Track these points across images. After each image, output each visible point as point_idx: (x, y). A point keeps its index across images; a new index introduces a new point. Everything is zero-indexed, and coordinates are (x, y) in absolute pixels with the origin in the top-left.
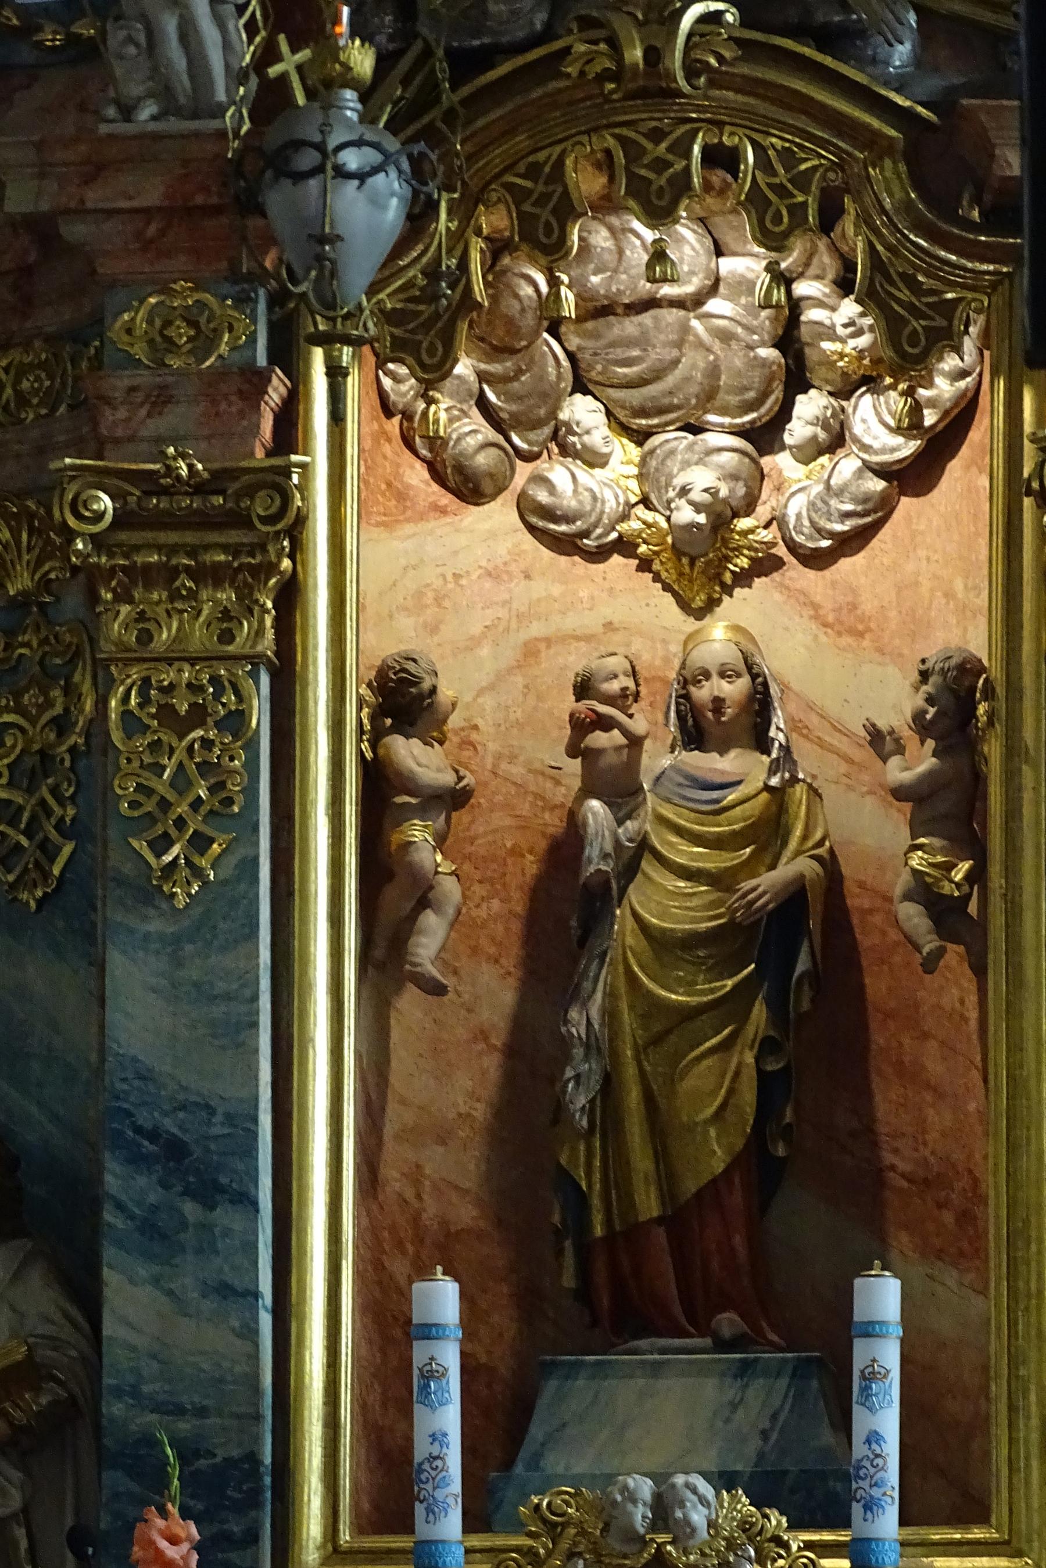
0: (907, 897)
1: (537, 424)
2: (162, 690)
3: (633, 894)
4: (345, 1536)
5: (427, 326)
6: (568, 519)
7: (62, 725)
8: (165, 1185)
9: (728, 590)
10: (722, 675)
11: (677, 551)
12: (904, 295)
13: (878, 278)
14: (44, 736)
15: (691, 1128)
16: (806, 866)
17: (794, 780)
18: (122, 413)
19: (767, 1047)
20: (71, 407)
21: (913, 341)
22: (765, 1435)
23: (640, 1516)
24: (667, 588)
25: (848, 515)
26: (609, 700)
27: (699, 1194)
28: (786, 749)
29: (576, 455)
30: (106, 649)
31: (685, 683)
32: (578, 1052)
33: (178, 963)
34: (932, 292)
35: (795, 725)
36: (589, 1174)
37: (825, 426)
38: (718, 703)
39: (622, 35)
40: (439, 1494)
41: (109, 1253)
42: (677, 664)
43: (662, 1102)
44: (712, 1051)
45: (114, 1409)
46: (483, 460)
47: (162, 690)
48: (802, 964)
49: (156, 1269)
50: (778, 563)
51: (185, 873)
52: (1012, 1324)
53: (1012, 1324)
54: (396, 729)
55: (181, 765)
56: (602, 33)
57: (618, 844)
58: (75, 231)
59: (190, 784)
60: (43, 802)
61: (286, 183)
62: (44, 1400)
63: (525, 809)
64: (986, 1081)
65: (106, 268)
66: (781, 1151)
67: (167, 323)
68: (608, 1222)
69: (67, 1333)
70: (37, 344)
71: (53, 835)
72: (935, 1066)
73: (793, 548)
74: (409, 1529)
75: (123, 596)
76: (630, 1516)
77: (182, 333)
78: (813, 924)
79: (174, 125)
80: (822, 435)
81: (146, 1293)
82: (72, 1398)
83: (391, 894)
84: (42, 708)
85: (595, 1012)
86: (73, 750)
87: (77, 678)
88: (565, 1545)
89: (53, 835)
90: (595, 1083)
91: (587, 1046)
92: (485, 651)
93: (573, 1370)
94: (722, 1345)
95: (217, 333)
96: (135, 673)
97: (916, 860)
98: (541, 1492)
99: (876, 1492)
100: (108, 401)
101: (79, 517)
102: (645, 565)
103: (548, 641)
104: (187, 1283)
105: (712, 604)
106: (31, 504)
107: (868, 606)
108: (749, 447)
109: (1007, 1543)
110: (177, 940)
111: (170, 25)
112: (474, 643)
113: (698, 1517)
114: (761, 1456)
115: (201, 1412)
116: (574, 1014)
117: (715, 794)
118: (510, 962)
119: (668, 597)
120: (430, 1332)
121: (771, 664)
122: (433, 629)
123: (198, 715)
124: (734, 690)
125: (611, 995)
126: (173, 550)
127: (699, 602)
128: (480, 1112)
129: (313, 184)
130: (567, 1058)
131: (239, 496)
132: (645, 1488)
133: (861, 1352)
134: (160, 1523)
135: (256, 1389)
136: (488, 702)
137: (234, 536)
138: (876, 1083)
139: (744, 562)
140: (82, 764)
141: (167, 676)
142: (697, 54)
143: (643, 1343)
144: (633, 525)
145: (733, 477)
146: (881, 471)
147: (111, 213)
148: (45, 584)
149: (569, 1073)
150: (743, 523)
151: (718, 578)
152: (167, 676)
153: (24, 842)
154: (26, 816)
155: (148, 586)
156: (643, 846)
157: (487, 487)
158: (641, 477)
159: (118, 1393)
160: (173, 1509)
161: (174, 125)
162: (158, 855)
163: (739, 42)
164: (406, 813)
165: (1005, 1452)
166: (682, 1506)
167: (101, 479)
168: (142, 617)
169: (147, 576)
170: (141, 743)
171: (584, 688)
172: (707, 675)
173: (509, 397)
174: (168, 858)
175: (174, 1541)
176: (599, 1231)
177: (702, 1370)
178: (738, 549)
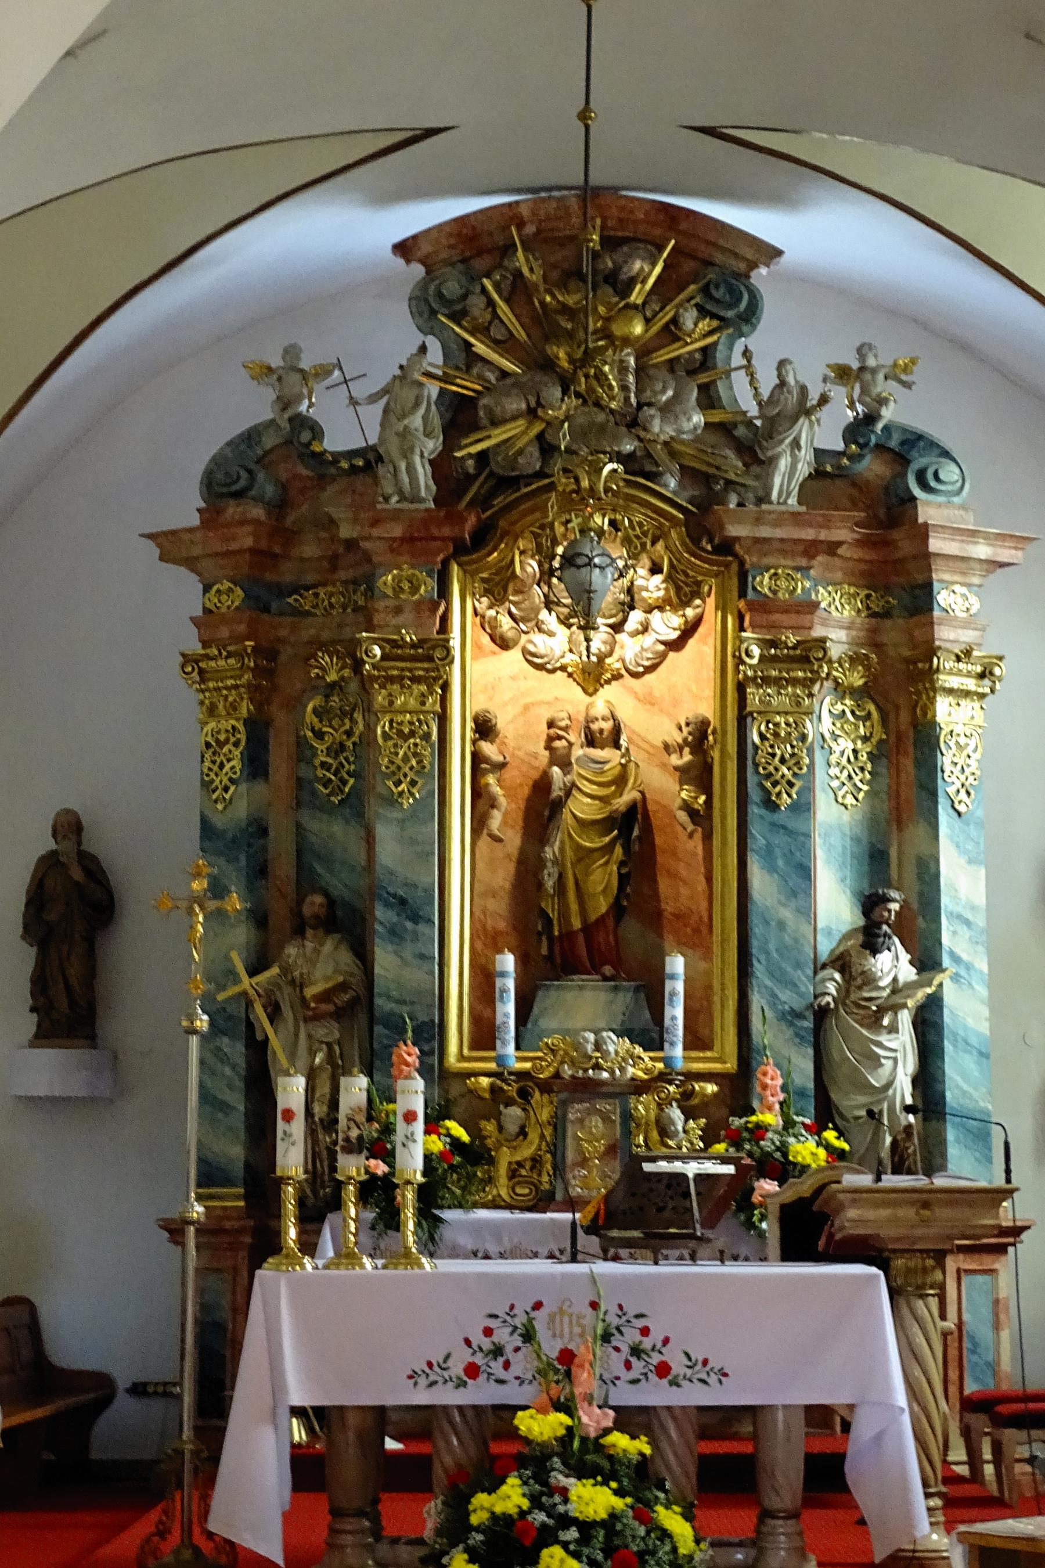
0: (680, 808)
1: (529, 620)
2: (398, 723)
3: (569, 802)
4: (466, 1052)
5: (497, 584)
6: (542, 657)
7: (349, 733)
8: (398, 915)
9: (602, 686)
10: (603, 719)
11: (583, 671)
12: (683, 578)
13: (673, 571)
14: (339, 736)
15: (594, 895)
16: (636, 795)
17: (630, 760)
18: (382, 615)
19: (622, 864)
20: (353, 611)
21: (686, 595)
22: (624, 1014)
23: (590, 1047)
24: (578, 684)
25: (648, 659)
26: (561, 729)
27: (597, 921)
28: (627, 749)
29: (544, 632)
30: (376, 707)
31: (587, 722)
32: (549, 864)
33: (403, 829)
34: (693, 577)
35: (630, 740)
36: (553, 910)
37: (642, 624)
38: (601, 731)
39: (581, 477)
40: (507, 1037)
41: (377, 941)
42: (584, 714)
43: (581, 884)
44: (602, 865)
45: (378, 1001)
46: (510, 634)
47: (398, 723)
48: (636, 833)
49: (395, 947)
50: (621, 676)
51: (407, 794)
52: (723, 973)
53: (723, 973)
54: (481, 738)
55: (405, 753)
56: (571, 475)
57: (565, 784)
58: (366, 545)
59: (409, 760)
60: (341, 764)
61: (573, 569)
62: (348, 996)
63: (524, 769)
64: (709, 879)
65: (376, 559)
66: (625, 903)
67: (400, 581)
68: (560, 931)
69: (355, 970)
70: (338, 583)
71: (346, 776)
72: (683, 872)
73: (627, 670)
74: (494, 1048)
75: (383, 686)
76: (586, 1049)
77: (406, 586)
78: (639, 816)
79: (405, 505)
80: (640, 628)
81: (392, 957)
82: (358, 994)
83: (482, 803)
84: (341, 726)
85: (556, 849)
86: (354, 744)
87: (355, 715)
88: (559, 1058)
89: (346, 776)
90: (556, 876)
91: (553, 862)
92: (509, 708)
93: (548, 987)
94: (606, 979)
95: (420, 586)
96: (387, 718)
97: (684, 795)
98: (548, 1038)
99: (675, 1039)
100: (377, 611)
101: (368, 656)
102: (570, 675)
103: (533, 704)
104: (407, 954)
105: (596, 691)
106: (339, 647)
107: (656, 693)
108: (611, 631)
109: (720, 1058)
110: (404, 820)
111: (403, 466)
112: (506, 704)
113: (611, 1048)
114: (623, 1022)
115: (413, 1003)
116: (547, 849)
117: (600, 766)
118: (518, 828)
119: (579, 689)
120: (503, 974)
121: (620, 715)
122: (491, 699)
123: (412, 734)
124: (607, 726)
125: (562, 842)
126: (403, 670)
127: (591, 690)
128: (507, 885)
129: (583, 570)
130: (545, 866)
131: (429, 649)
132: (591, 1037)
133: (668, 985)
134: (405, 1048)
135: (434, 994)
136: (511, 727)
137: (426, 665)
138: (659, 878)
139: (609, 675)
140: (358, 749)
141: (400, 718)
142: (609, 484)
143: (575, 977)
144: (563, 661)
145: (605, 643)
146: (663, 643)
147: (380, 538)
148: (343, 678)
149: (546, 872)
150: (608, 661)
151: (598, 681)
152: (400, 718)
153: (333, 778)
154: (334, 767)
155: (392, 683)
156: (574, 785)
157: (511, 644)
158: (569, 642)
159: (380, 995)
160: (409, 1042)
161: (405, 505)
162: (396, 787)
163: (625, 480)
164: (486, 772)
165: (719, 1024)
166: (606, 1044)
167: (375, 641)
168: (390, 695)
169: (391, 679)
170: (390, 743)
171: (551, 724)
172: (597, 719)
173: (519, 609)
174: (400, 789)
175: (409, 1055)
176: (556, 933)
177: (595, 989)
178: (607, 671)
